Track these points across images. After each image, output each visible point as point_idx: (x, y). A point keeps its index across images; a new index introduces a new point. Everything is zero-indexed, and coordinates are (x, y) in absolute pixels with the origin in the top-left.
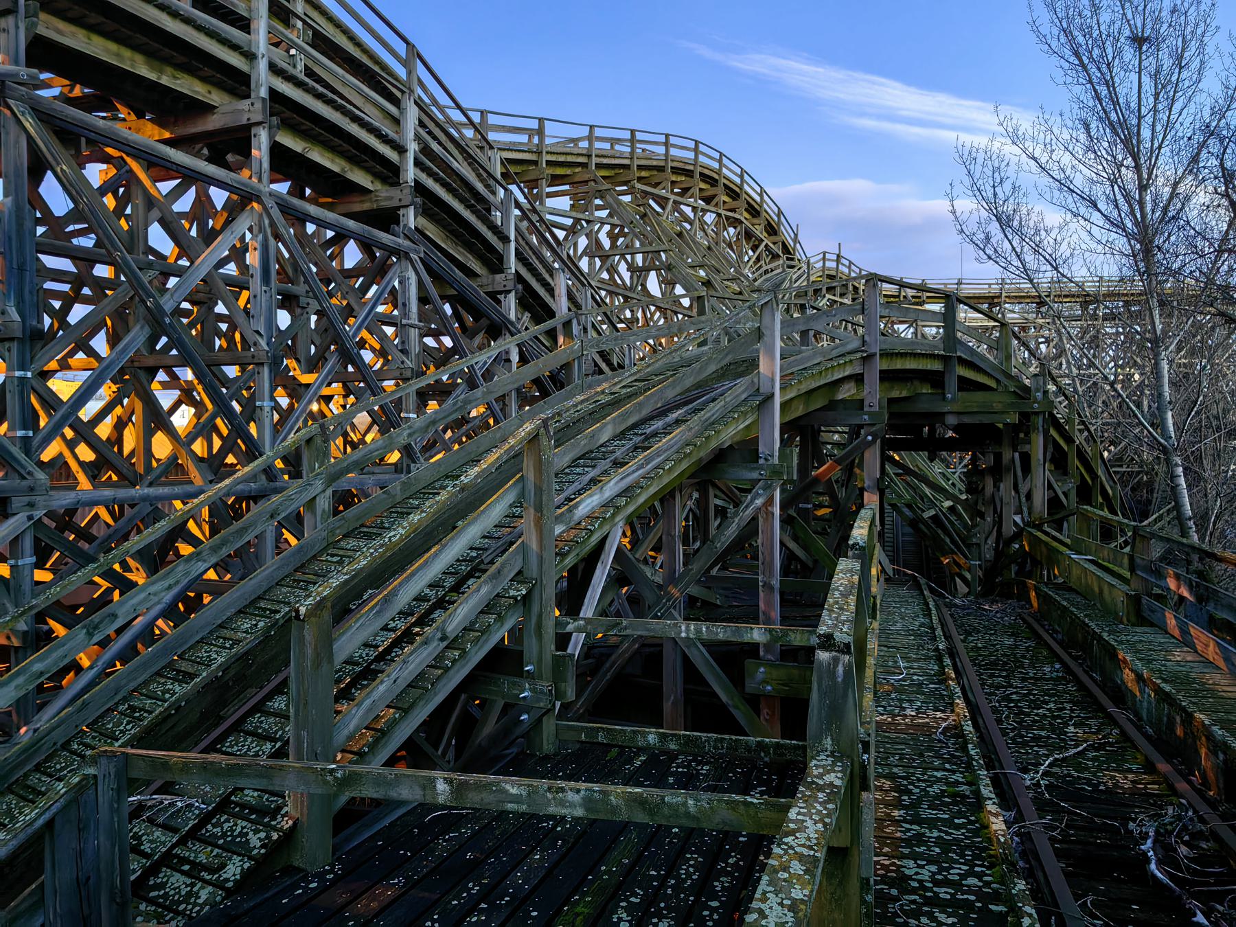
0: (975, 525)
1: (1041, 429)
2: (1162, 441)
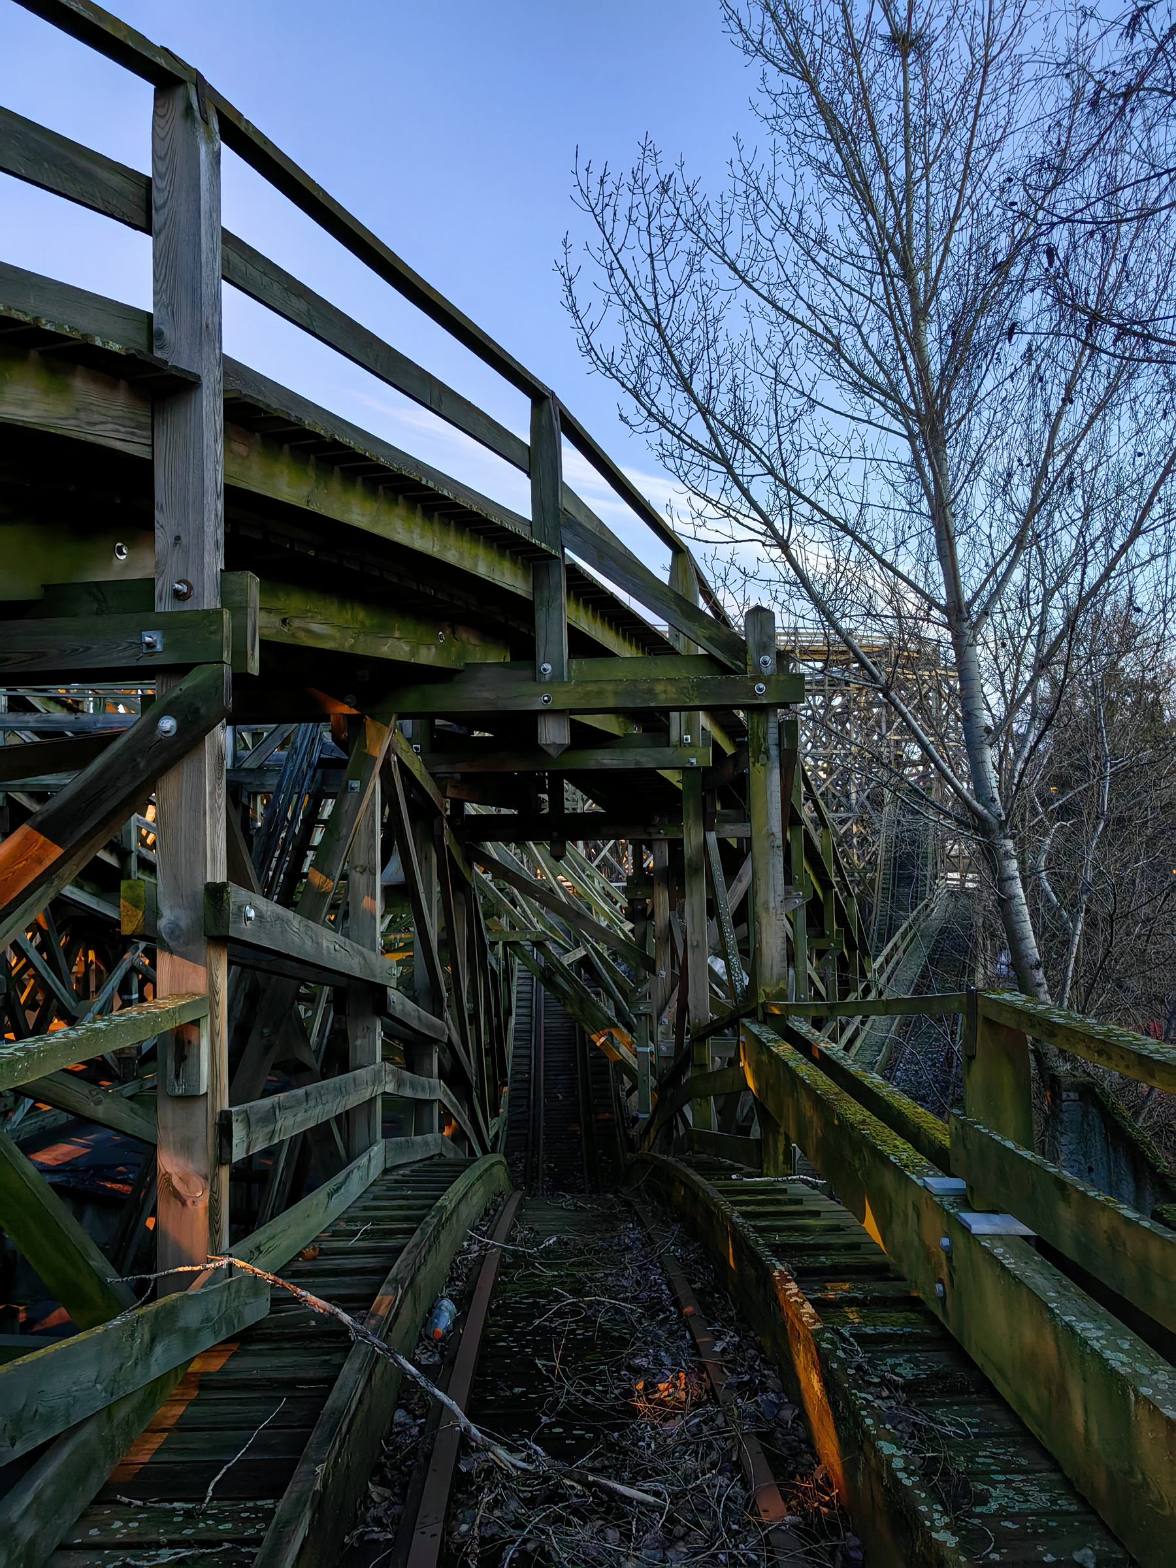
0: (640, 982)
1: (774, 752)
2: (980, 807)
